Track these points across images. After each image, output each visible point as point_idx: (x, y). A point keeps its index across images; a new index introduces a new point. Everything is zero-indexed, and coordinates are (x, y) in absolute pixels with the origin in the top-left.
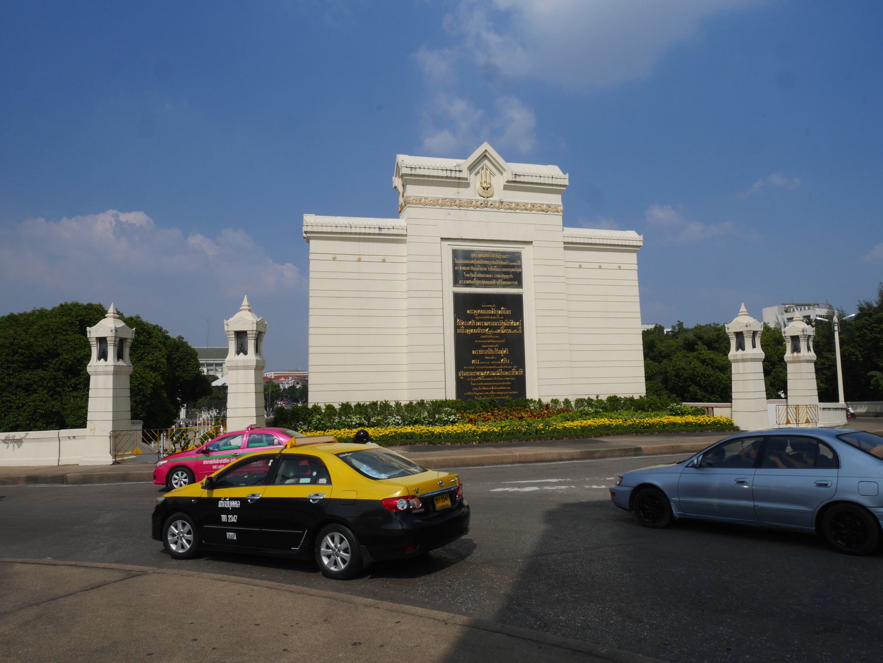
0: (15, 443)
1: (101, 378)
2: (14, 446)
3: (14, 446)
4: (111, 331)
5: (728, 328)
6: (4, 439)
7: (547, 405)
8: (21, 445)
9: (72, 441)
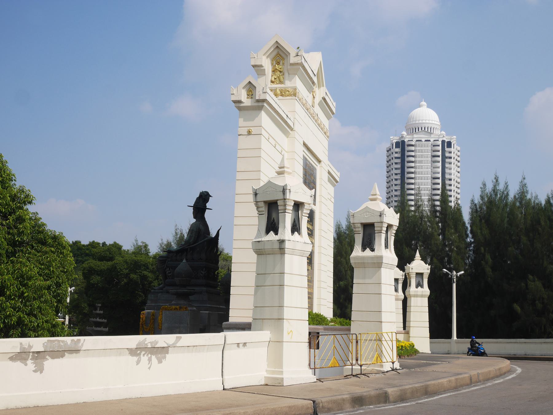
0: (151, 354)
1: (296, 258)
2: (150, 360)
3: (150, 360)
4: (311, 196)
5: (412, 269)
6: (134, 346)
7: (20, 219)
8: (165, 358)
9: (242, 350)
